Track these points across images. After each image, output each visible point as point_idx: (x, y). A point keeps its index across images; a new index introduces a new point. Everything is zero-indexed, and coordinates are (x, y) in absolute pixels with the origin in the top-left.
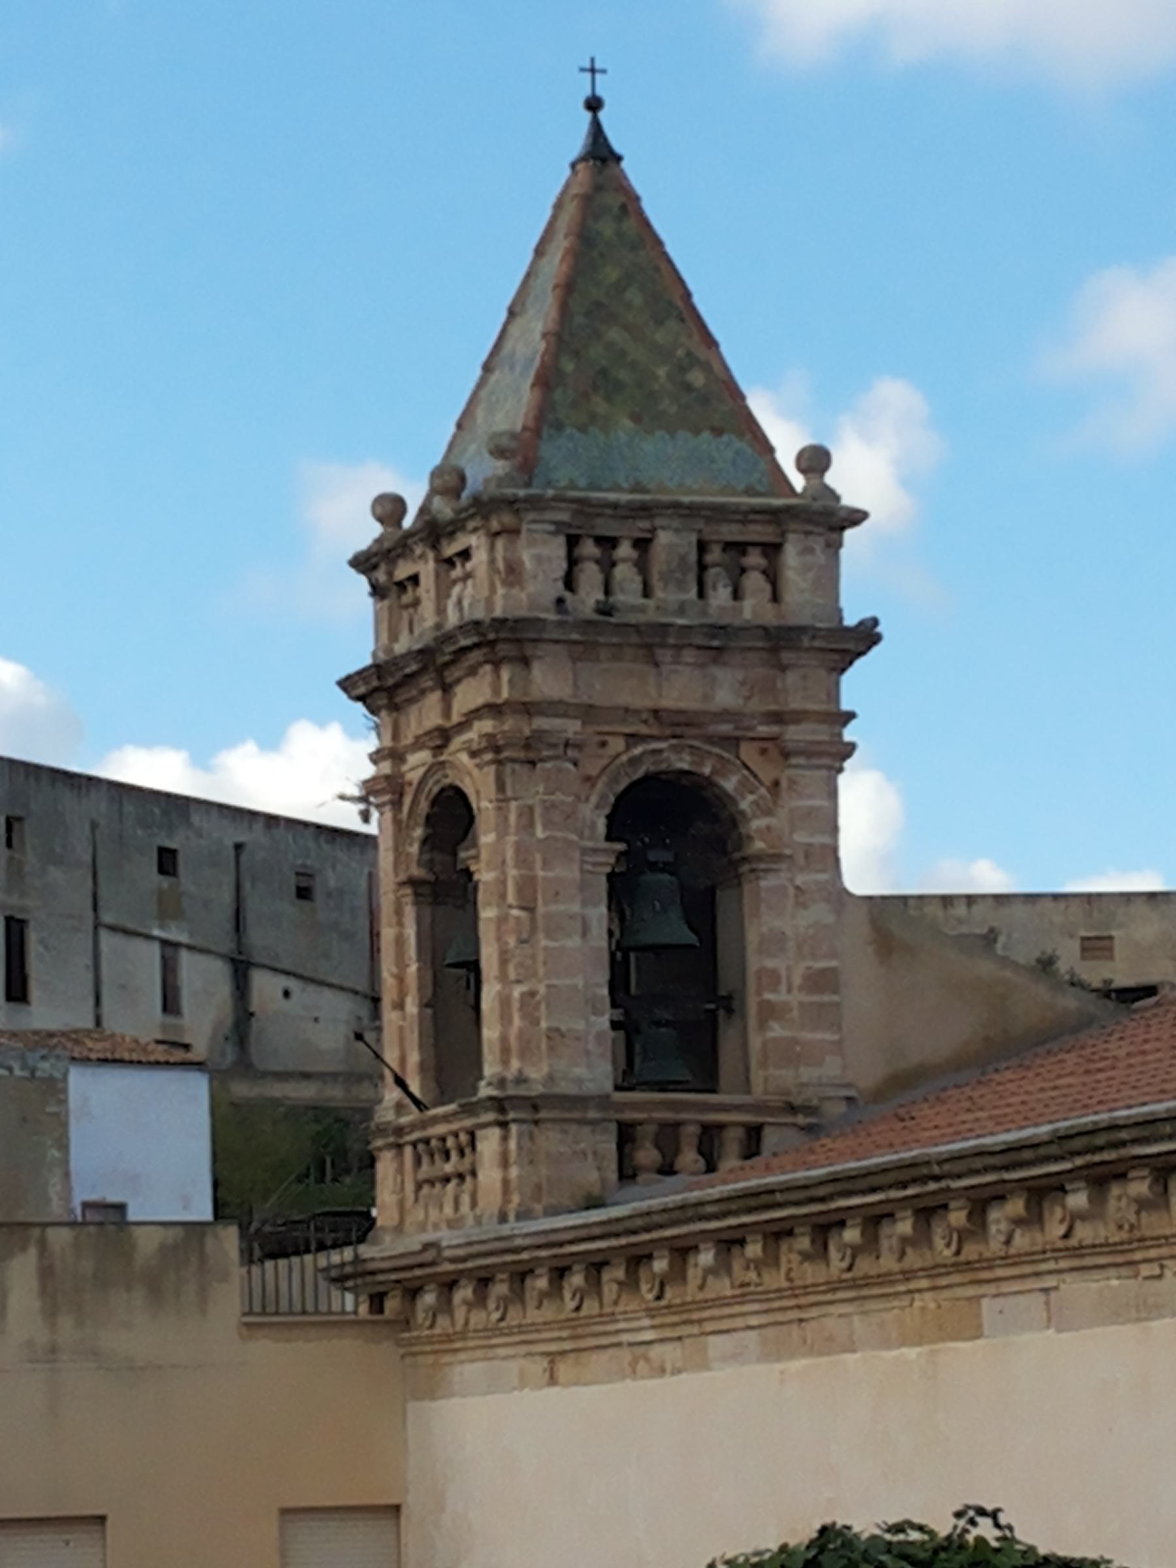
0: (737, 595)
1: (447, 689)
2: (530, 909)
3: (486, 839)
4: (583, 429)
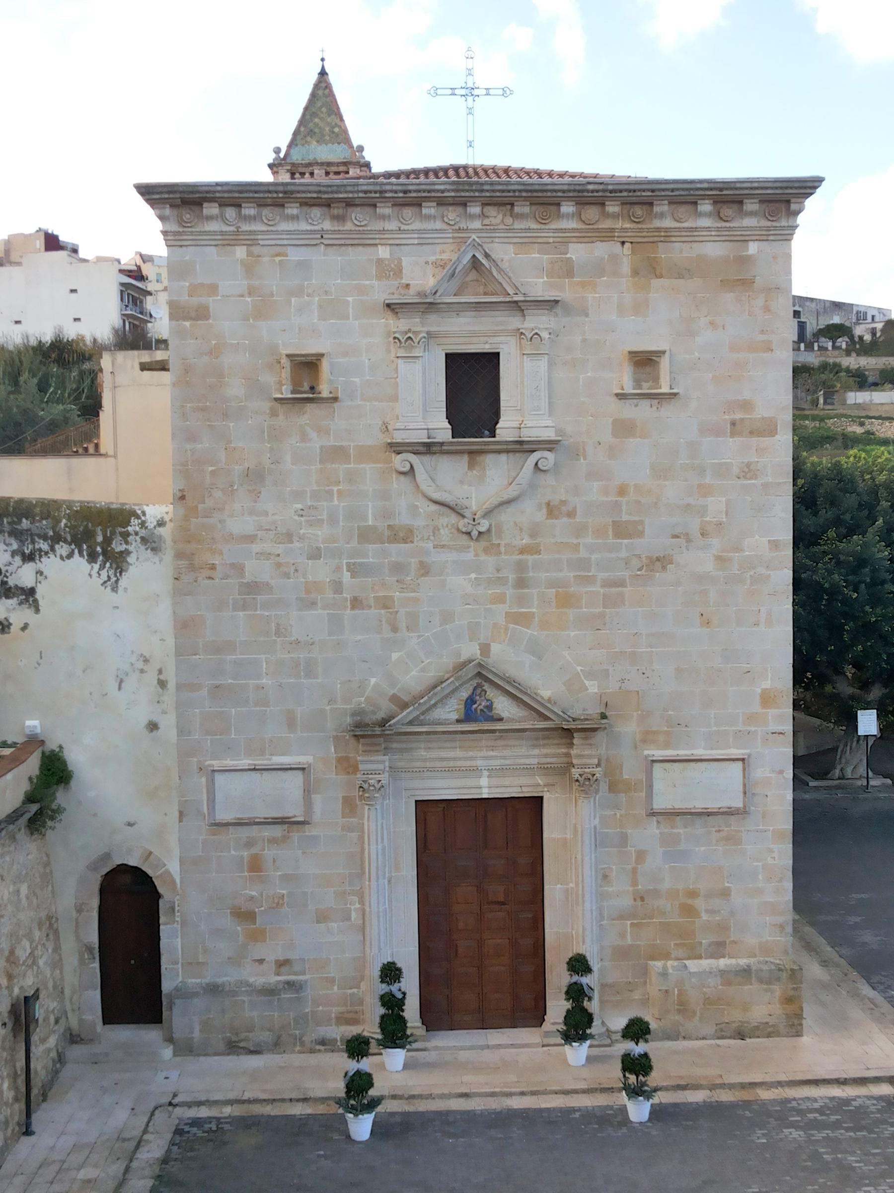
4: (303, 145)
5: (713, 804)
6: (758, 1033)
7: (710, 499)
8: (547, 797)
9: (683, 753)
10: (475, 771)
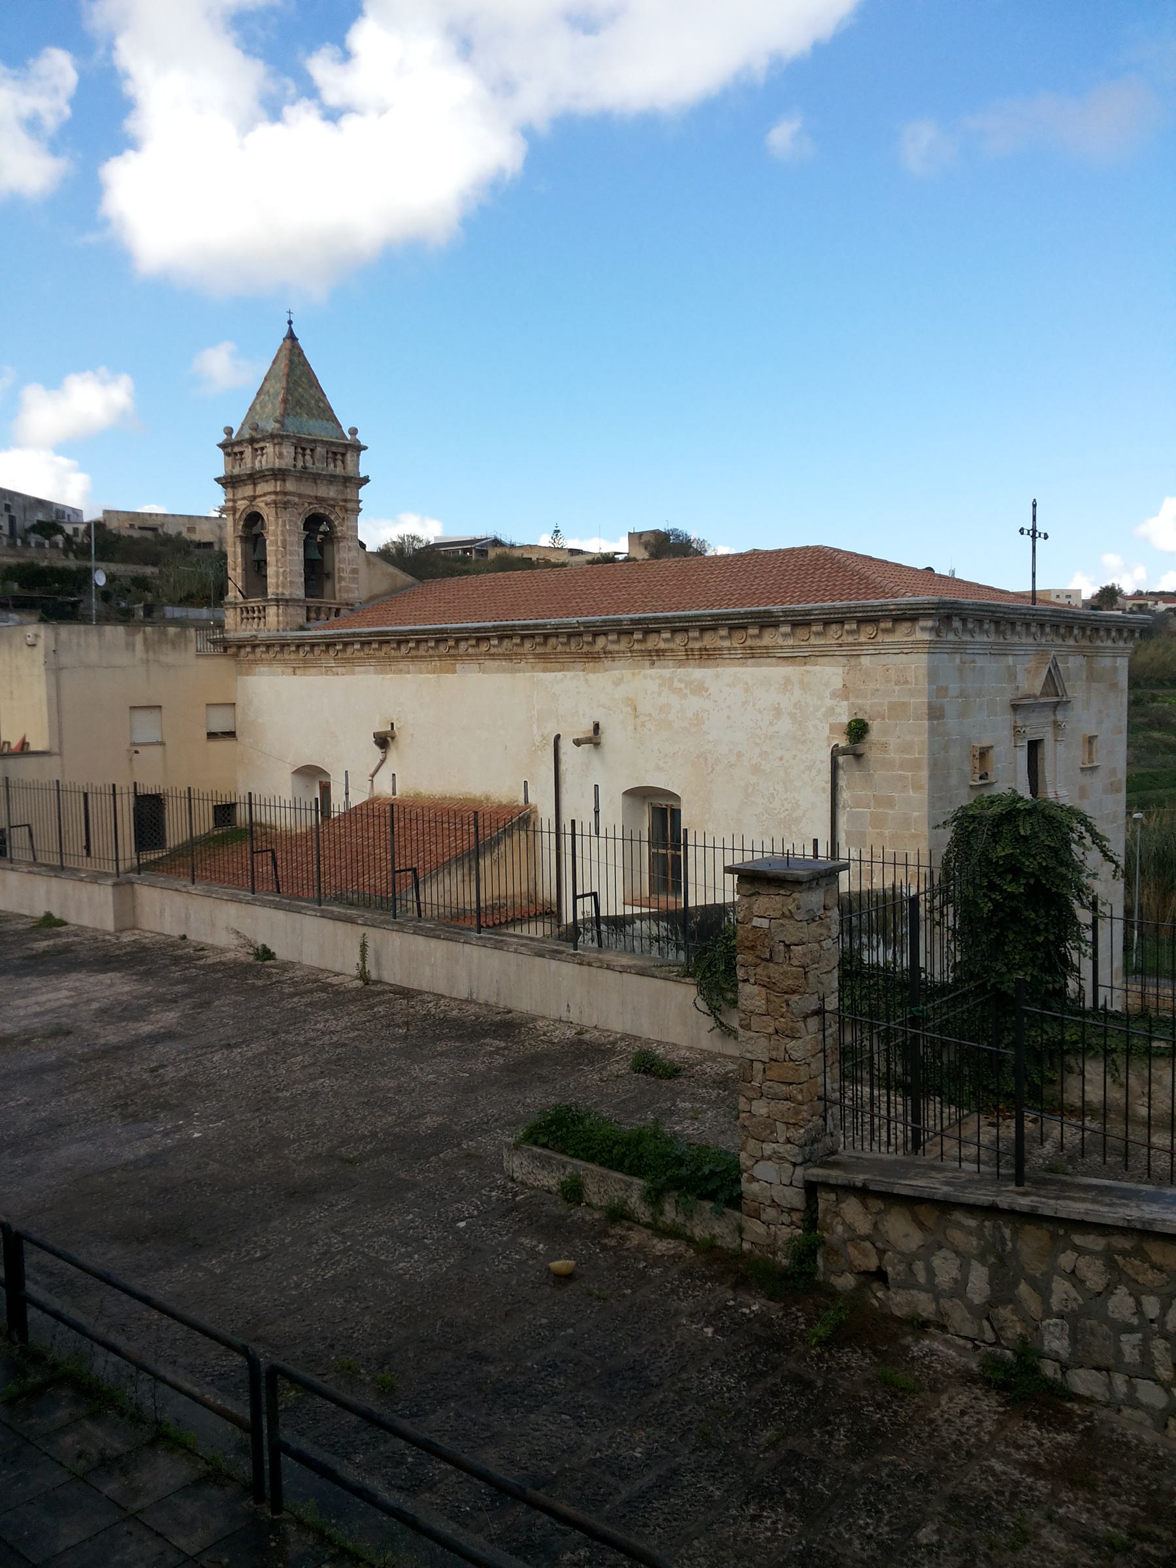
0: (335, 466)
1: (255, 485)
2: (285, 548)
3: (271, 528)
4: (295, 416)
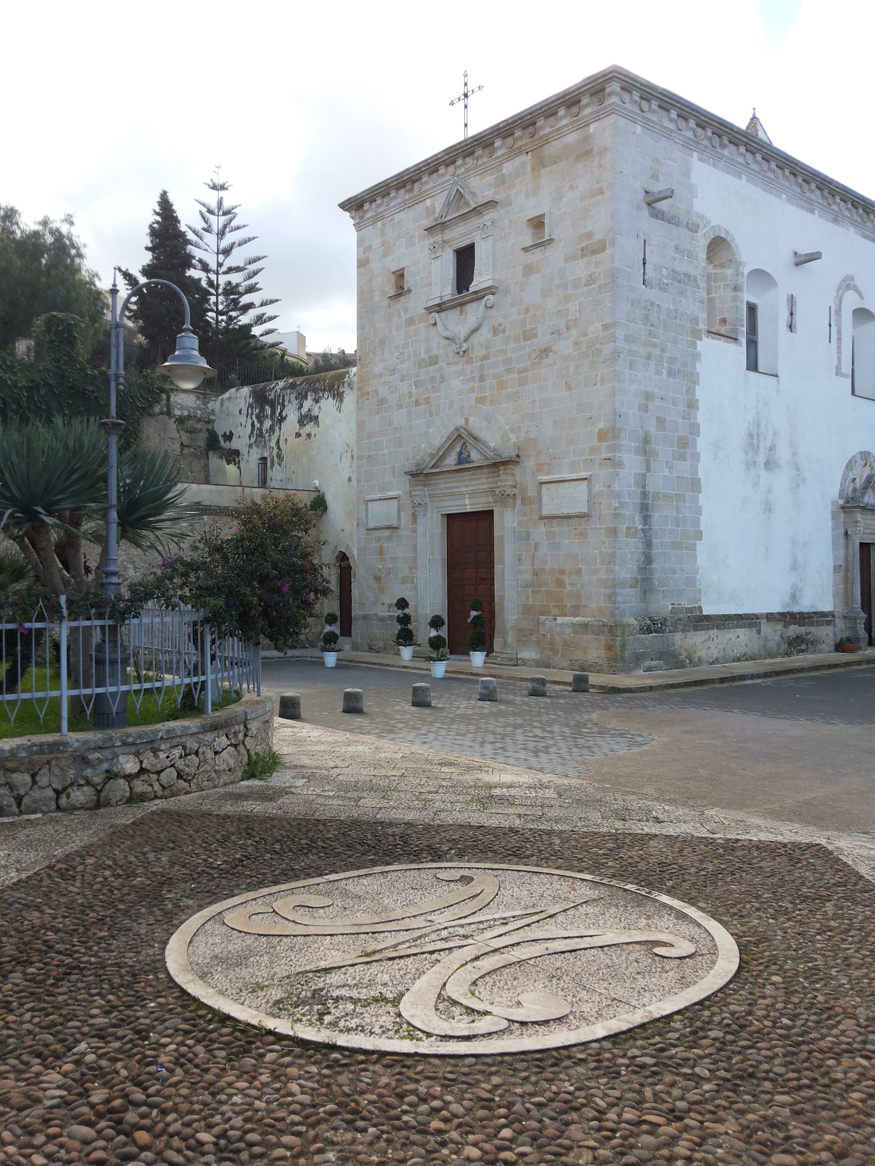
5: (572, 511)
6: (592, 669)
7: (570, 304)
8: (495, 509)
9: (557, 477)
10: (462, 495)
